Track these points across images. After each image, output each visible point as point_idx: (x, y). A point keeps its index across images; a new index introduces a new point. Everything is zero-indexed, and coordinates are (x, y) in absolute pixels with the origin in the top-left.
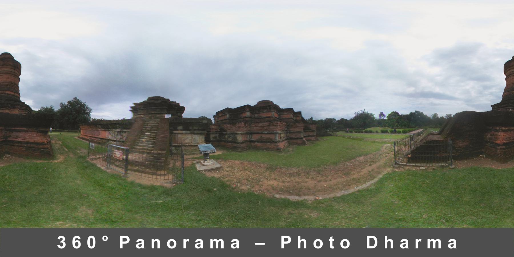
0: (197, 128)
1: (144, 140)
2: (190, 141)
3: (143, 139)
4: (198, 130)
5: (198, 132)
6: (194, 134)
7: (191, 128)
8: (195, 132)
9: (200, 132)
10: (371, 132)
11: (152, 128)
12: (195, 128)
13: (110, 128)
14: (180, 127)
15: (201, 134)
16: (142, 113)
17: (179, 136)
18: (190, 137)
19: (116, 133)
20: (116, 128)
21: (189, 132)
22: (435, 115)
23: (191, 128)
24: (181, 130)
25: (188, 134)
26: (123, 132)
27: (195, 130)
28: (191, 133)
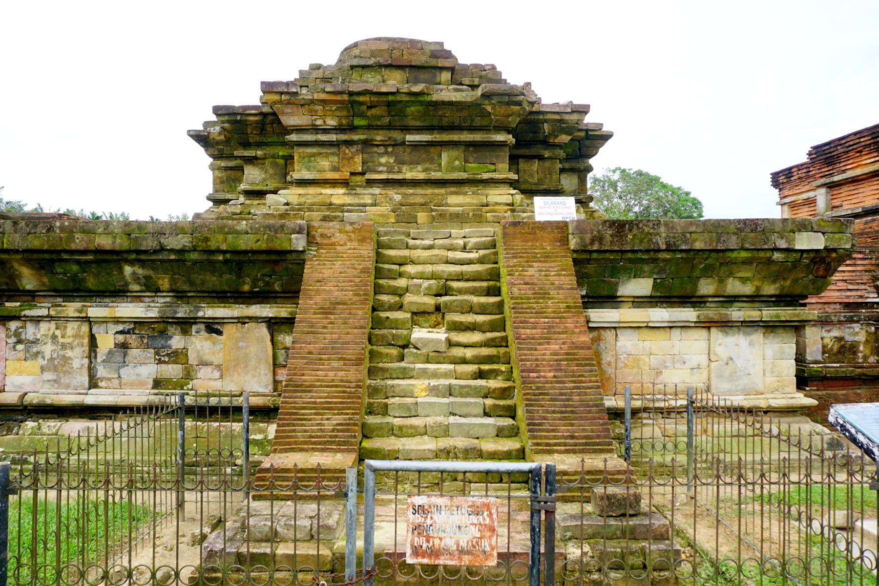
0: (748, 289)
1: (420, 385)
2: (697, 381)
3: (405, 374)
4: (754, 299)
5: (753, 314)
6: (725, 325)
7: (706, 287)
8: (736, 313)
9: (768, 313)
10: (804, 305)
11: (446, 291)
12: (734, 287)
13: (31, 296)
14: (642, 286)
15: (770, 327)
16: (325, 165)
17: (627, 342)
18: (694, 345)
19: (107, 341)
20: (119, 293)
21: (689, 314)
22: (301, 72)
23: (706, 287)
24: (639, 302)
25: (685, 327)
26: (185, 325)
27: (732, 300)
28: (707, 325)
